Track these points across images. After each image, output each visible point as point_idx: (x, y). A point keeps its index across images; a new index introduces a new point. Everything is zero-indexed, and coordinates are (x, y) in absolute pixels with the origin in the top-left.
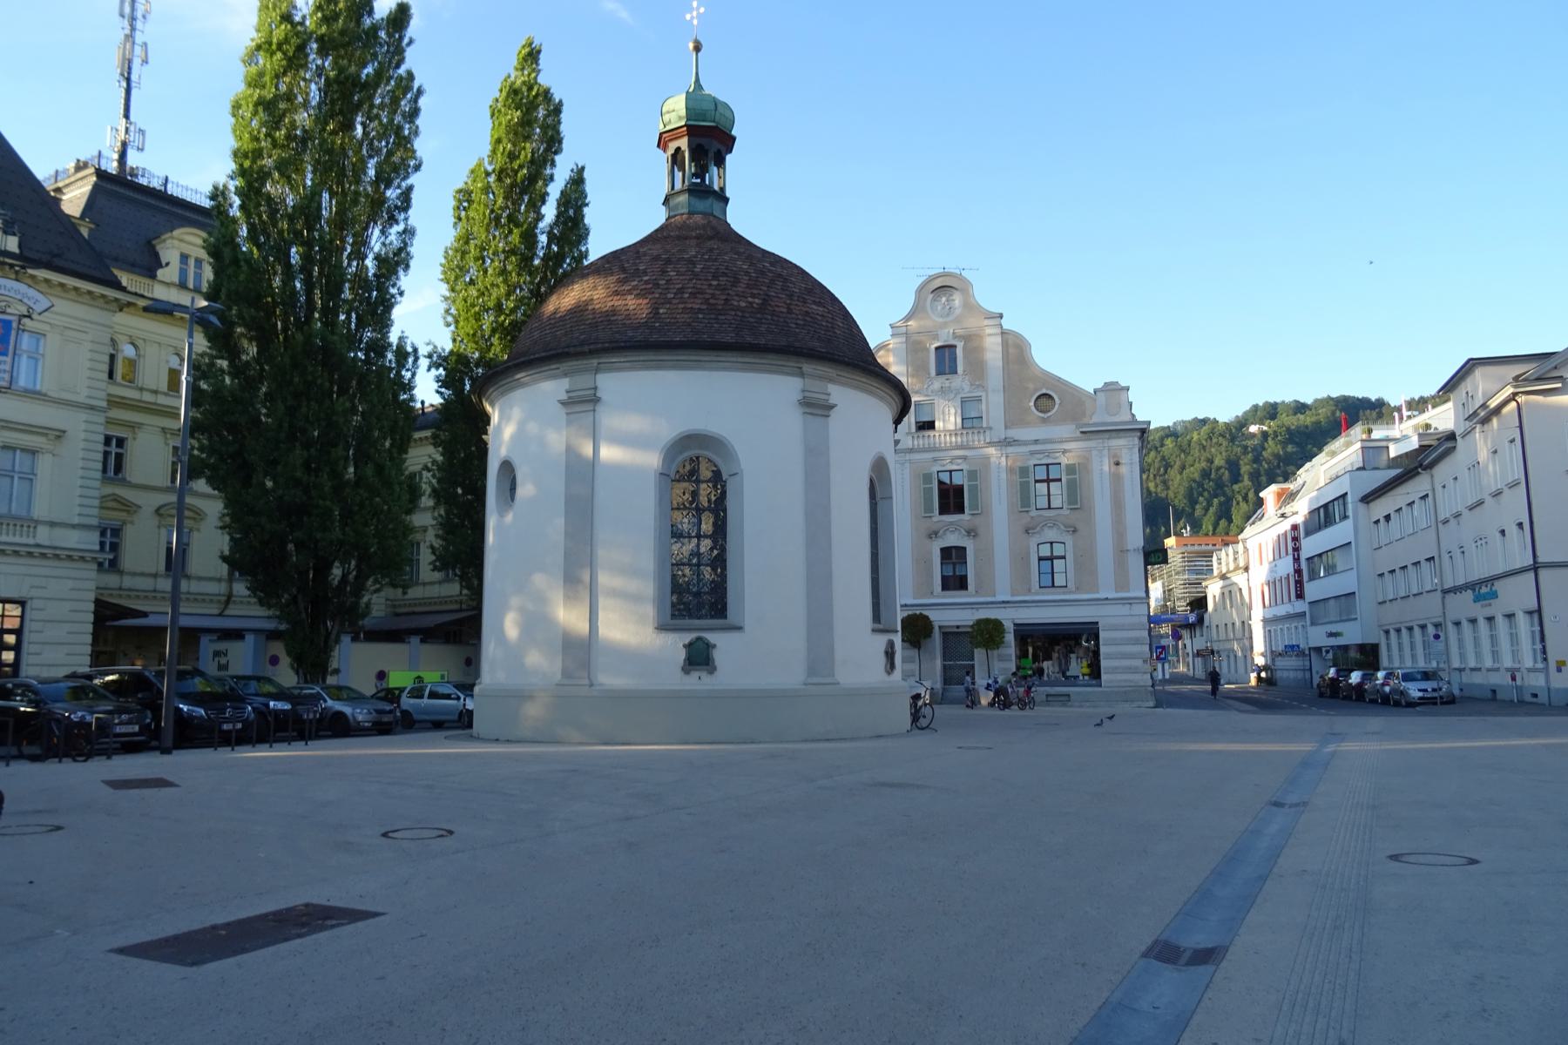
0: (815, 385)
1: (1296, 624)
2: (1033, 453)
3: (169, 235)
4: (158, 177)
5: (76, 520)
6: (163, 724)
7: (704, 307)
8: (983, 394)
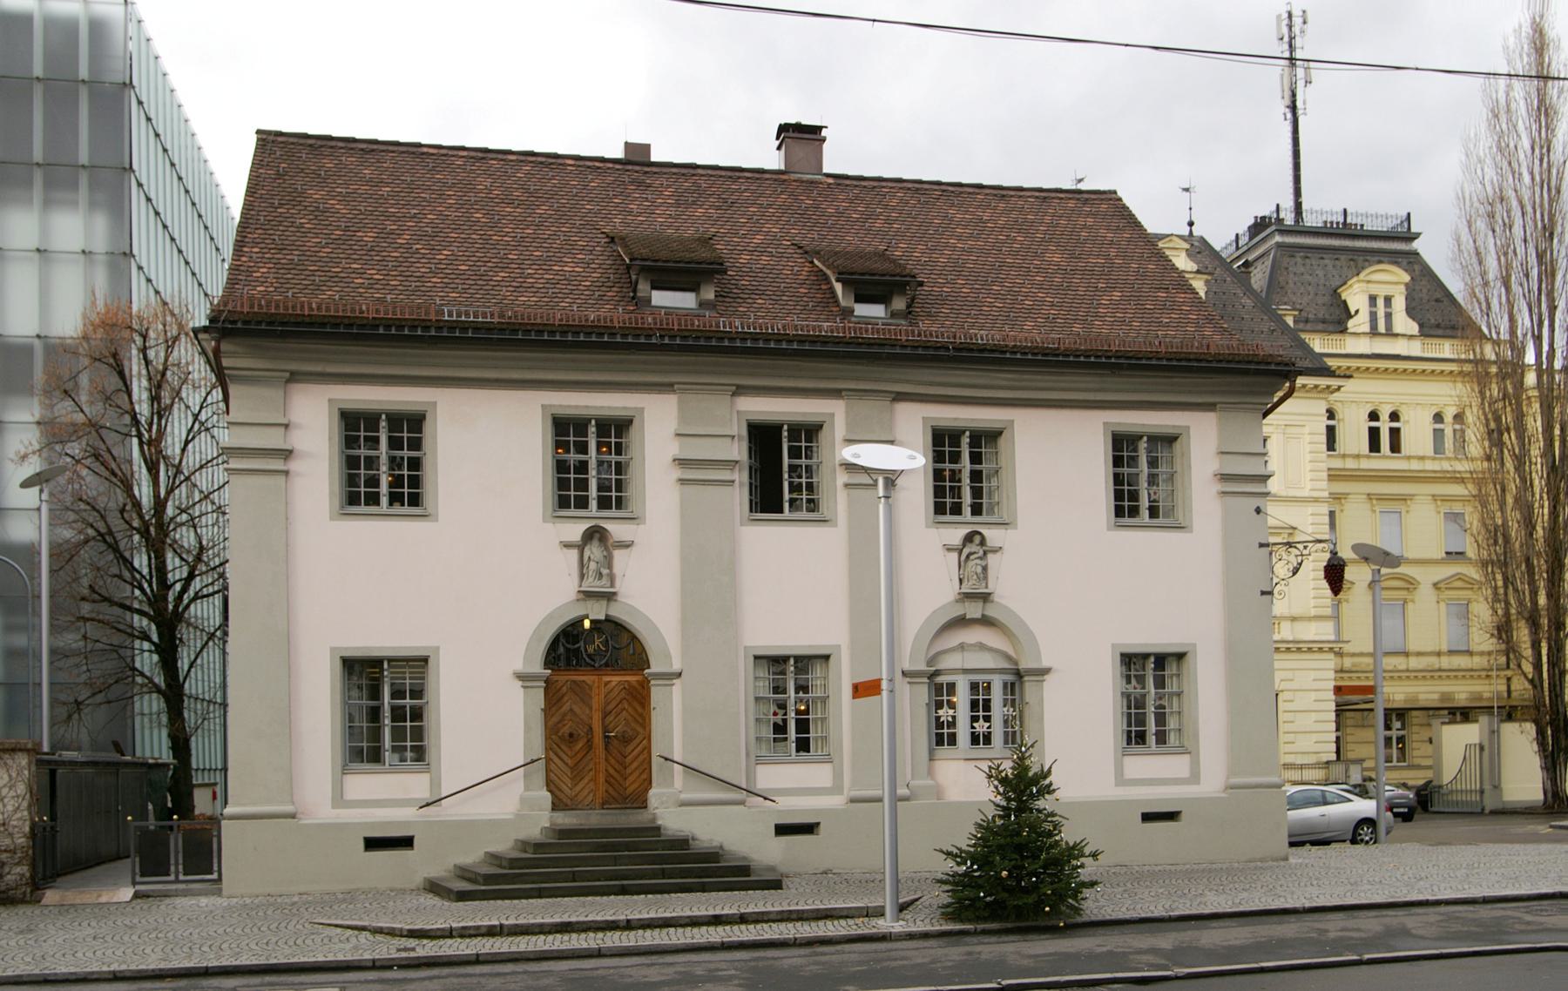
3: (1355, 279)
4: (1337, 213)
5: (1313, 612)
6: (150, 807)
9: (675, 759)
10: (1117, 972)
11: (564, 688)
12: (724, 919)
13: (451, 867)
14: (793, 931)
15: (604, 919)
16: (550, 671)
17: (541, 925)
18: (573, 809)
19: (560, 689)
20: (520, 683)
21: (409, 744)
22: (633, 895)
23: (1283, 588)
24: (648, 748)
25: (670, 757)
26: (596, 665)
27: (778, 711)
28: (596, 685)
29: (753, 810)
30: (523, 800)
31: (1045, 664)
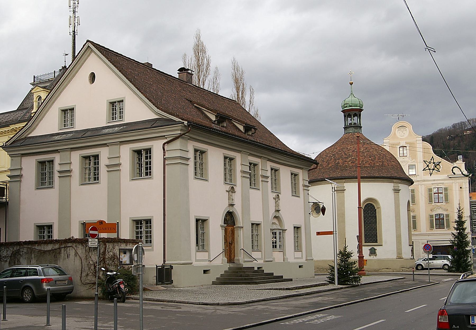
0: (396, 185)
1: (277, 256)
2: (433, 184)
7: (369, 166)
8: (416, 164)
10: (295, 314)
20: (221, 228)
23: (313, 213)
31: (286, 229)
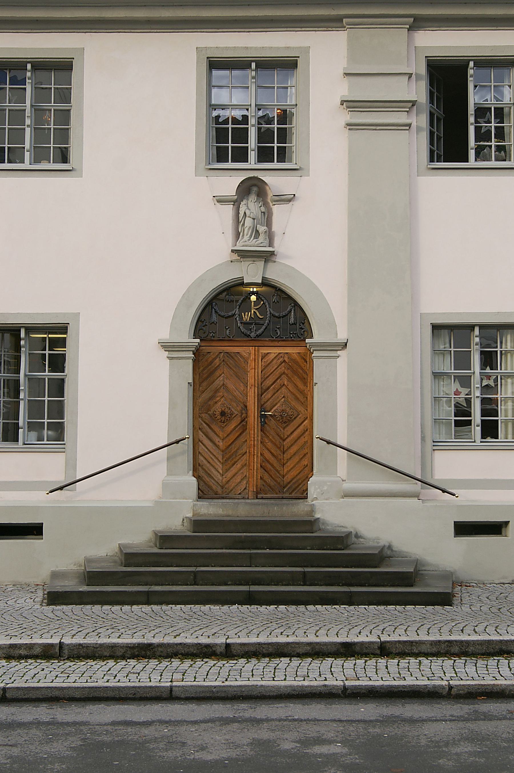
9: (339, 443)
11: (217, 362)
12: (357, 649)
13: (82, 560)
14: (450, 673)
15: (196, 641)
16: (198, 340)
17: (113, 647)
18: (223, 498)
19: (212, 362)
21: (46, 421)
22: (261, 604)
24: (309, 430)
25: (332, 440)
26: (253, 335)
27: (460, 389)
28: (252, 357)
29: (428, 504)
30: (165, 485)
